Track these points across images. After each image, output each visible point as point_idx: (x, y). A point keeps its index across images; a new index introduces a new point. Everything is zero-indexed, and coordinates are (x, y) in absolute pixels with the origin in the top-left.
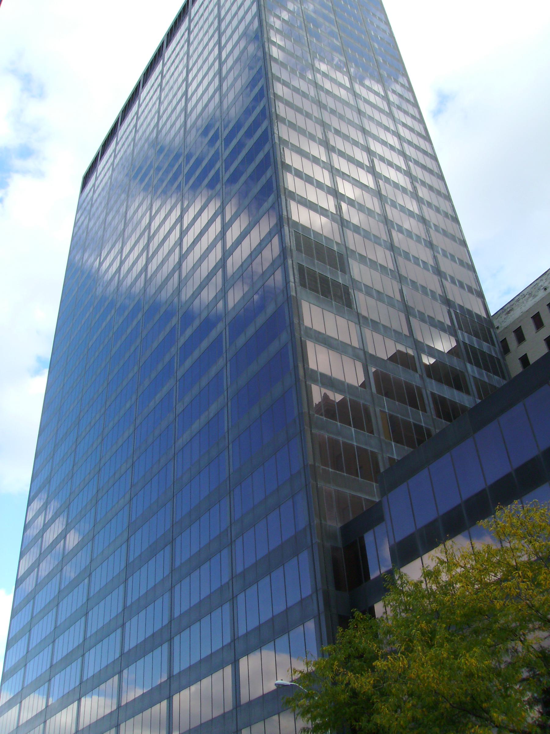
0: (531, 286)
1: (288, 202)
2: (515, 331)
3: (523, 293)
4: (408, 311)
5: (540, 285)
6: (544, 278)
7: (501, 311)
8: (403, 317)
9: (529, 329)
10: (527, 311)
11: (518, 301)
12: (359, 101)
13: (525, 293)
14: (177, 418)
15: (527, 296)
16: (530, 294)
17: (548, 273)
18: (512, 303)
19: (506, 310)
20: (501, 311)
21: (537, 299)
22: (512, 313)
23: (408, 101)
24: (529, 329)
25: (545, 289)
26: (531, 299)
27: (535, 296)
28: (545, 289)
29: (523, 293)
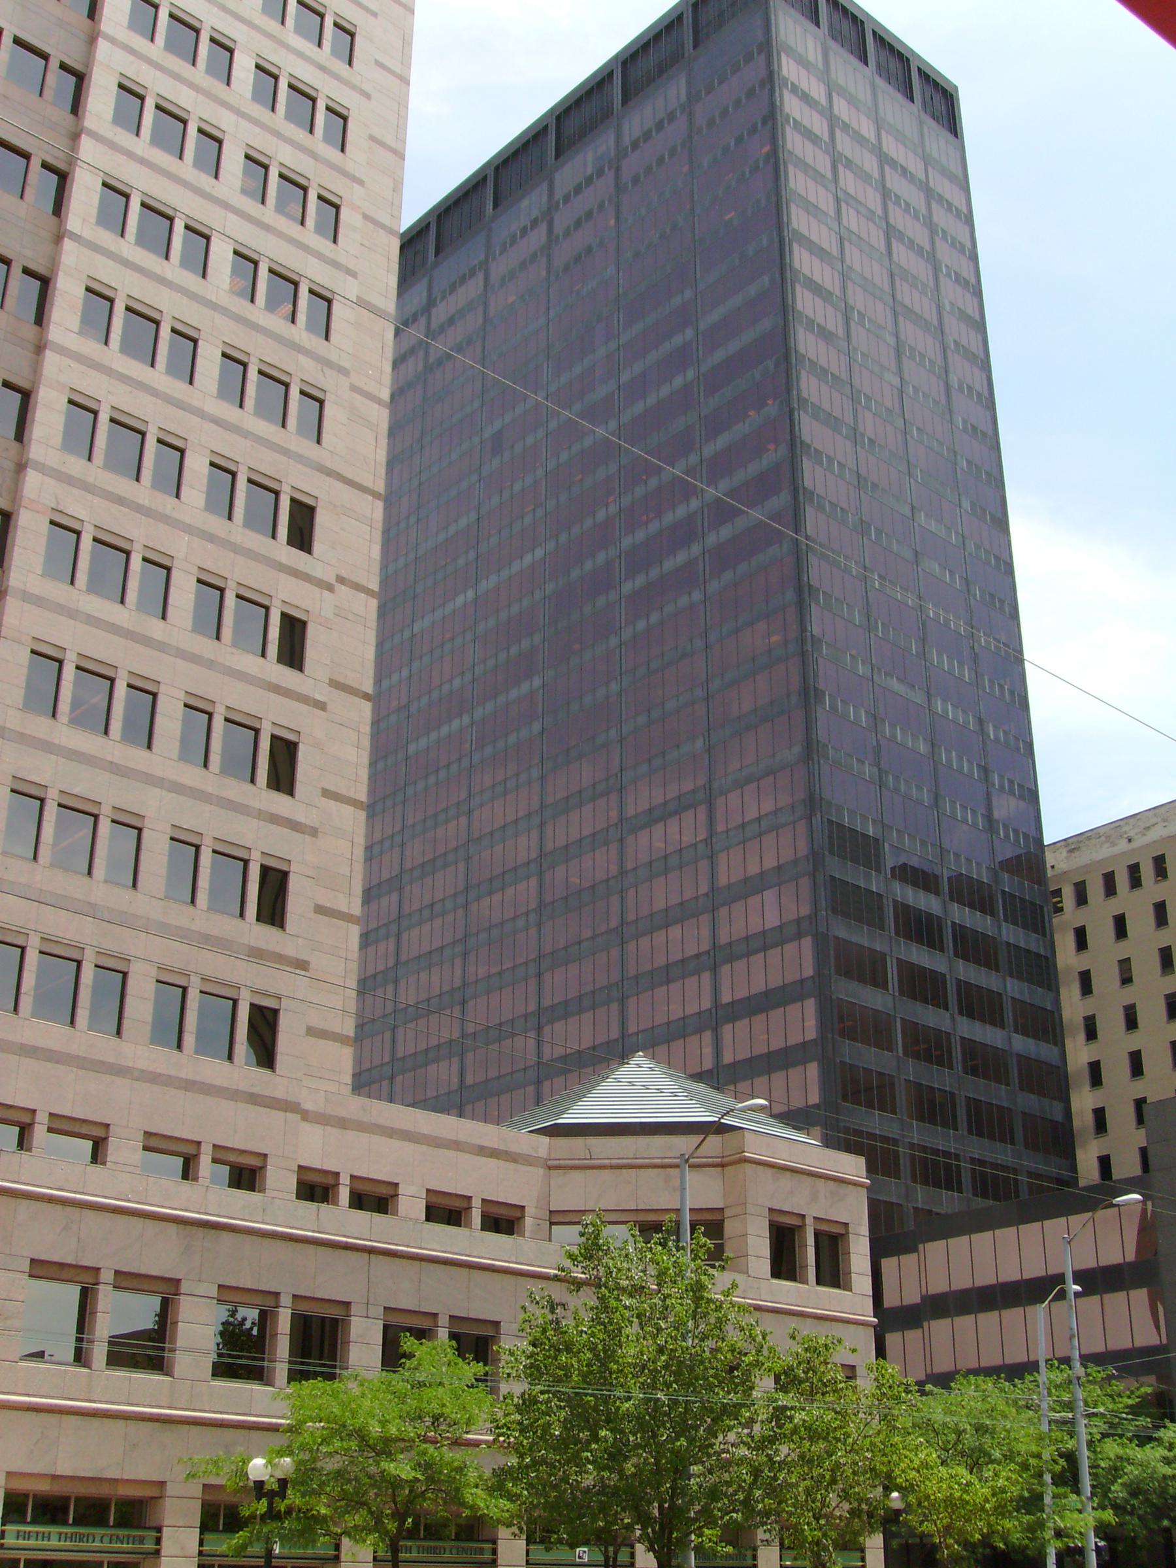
0: (1114, 825)
1: (860, 416)
2: (1076, 885)
3: (1099, 830)
4: (886, 194)
5: (1124, 830)
6: (1131, 821)
7: (1063, 843)
8: (878, 197)
9: (1095, 890)
10: (1098, 862)
11: (1089, 838)
12: (923, 177)
13: (1102, 831)
14: (698, 297)
15: (1103, 838)
16: (1108, 837)
17: (1138, 817)
18: (1080, 838)
19: (1073, 844)
20: (1063, 843)
21: (1116, 850)
22: (1077, 853)
23: (945, 173)
24: (1095, 890)
25: (1130, 841)
26: (1107, 845)
27: (1114, 844)
28: (1130, 841)
29: (1099, 830)
